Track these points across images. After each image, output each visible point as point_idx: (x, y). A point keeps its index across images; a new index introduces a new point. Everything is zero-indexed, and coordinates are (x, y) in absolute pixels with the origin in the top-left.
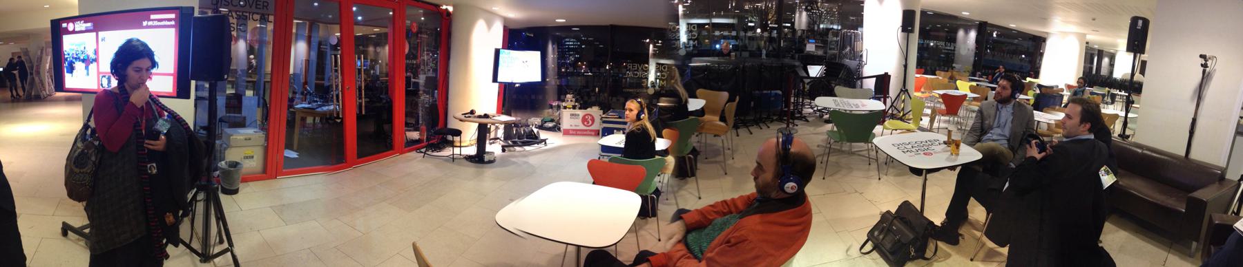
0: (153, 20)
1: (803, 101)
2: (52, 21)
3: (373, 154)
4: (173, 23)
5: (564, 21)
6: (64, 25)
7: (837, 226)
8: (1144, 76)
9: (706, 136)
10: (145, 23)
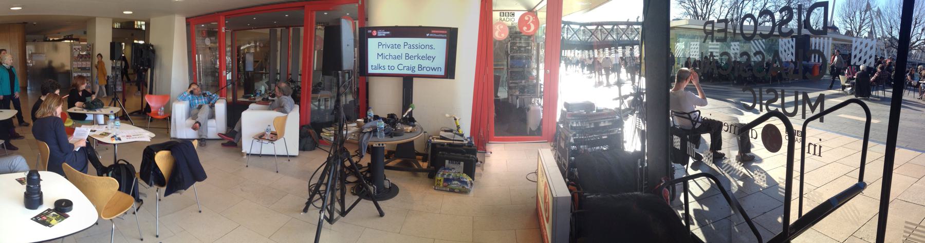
0: (433, 33)
2: (823, 122)
4: (445, 36)
5: (131, 13)
10: (428, 35)
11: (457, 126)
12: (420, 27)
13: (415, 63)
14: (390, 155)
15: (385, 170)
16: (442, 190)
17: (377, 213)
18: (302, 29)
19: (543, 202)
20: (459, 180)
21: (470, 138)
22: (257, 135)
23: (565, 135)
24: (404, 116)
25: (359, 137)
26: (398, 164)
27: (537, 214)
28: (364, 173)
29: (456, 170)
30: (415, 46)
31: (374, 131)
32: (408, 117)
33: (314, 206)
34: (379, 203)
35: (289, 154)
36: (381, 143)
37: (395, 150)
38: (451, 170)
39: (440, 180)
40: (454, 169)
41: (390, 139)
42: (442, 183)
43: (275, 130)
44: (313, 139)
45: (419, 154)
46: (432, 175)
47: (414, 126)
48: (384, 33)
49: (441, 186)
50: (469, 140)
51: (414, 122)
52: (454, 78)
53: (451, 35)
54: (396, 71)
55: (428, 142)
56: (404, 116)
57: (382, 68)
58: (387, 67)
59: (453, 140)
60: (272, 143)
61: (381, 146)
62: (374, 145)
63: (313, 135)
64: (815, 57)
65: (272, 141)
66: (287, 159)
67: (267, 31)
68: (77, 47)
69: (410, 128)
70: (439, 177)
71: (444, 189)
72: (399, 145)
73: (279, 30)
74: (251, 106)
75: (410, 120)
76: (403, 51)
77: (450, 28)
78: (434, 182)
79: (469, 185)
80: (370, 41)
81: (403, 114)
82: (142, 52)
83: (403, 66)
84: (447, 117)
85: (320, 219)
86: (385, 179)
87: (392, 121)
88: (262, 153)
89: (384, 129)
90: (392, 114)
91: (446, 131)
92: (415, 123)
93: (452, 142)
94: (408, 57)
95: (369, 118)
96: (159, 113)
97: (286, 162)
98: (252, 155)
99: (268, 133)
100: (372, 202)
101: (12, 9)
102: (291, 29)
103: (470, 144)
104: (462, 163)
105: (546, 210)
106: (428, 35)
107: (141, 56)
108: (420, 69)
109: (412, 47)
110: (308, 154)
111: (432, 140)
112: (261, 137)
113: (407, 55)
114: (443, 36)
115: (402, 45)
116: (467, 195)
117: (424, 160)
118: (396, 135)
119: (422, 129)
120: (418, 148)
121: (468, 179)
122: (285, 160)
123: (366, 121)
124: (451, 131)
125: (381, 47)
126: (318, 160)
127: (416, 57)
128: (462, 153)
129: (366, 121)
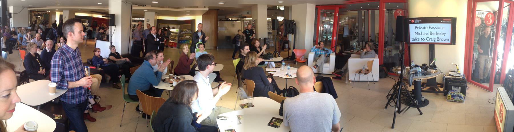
0: (444, 21)
1: (333, 38)
2: (12, 53)
3: (504, 127)
4: (450, 22)
8: (316, 82)
9: (393, 101)
10: (441, 22)
11: (457, 69)
12: (437, 17)
13: (435, 37)
14: (423, 85)
15: (422, 93)
16: (450, 101)
17: (419, 113)
18: (377, 12)
19: (499, 113)
20: (458, 96)
21: (464, 75)
22: (357, 71)
23: (512, 81)
24: (431, 65)
25: (408, 76)
26: (428, 89)
27: (494, 120)
29: (457, 91)
30: (435, 28)
31: (416, 73)
32: (433, 65)
33: (390, 105)
34: (420, 108)
35: (374, 80)
36: (420, 79)
37: (426, 82)
38: (454, 91)
39: (450, 96)
40: (456, 91)
41: (425, 77)
42: (450, 98)
43: (368, 69)
44: (385, 72)
45: (439, 84)
46: (445, 94)
47: (436, 70)
48: (418, 21)
49: (450, 99)
50: (463, 76)
51: (436, 68)
52: (455, 44)
53: (453, 21)
54: (425, 41)
55: (443, 78)
56: (431, 65)
57: (418, 39)
58: (420, 39)
59: (456, 76)
60: (366, 75)
61: (420, 80)
62: (416, 80)
63: (385, 70)
65: (366, 74)
66: (373, 83)
67: (356, 12)
68: (246, 22)
69: (434, 71)
70: (449, 95)
71: (452, 100)
72: (428, 80)
73: (363, 12)
74: (352, 55)
75: (434, 67)
76: (429, 30)
77: (453, 18)
78: (447, 98)
79: (463, 98)
81: (430, 64)
82: (289, 25)
83: (429, 38)
84: (452, 65)
85: (395, 111)
86: (422, 97)
87: (424, 68)
88: (360, 80)
89: (421, 72)
90: (424, 64)
91: (452, 72)
92: (437, 68)
93: (455, 77)
94: (432, 33)
95: (412, 66)
96: (301, 59)
97: (373, 84)
98: (355, 81)
99: (364, 70)
100: (416, 108)
102: (370, 11)
103: (463, 78)
104: (460, 88)
105: (500, 117)
106: (441, 22)
107: (289, 27)
108: (438, 40)
109: (433, 28)
110: (383, 80)
111: (445, 77)
112: (360, 72)
113: (431, 32)
114: (449, 22)
115: (428, 27)
116: (462, 103)
117: (441, 87)
118: (427, 75)
119: (440, 71)
120: (438, 81)
121: (463, 96)
122: (372, 84)
123: (411, 68)
124: (454, 72)
125: (417, 28)
126: (390, 84)
127: (436, 34)
128: (459, 82)
129: (411, 68)
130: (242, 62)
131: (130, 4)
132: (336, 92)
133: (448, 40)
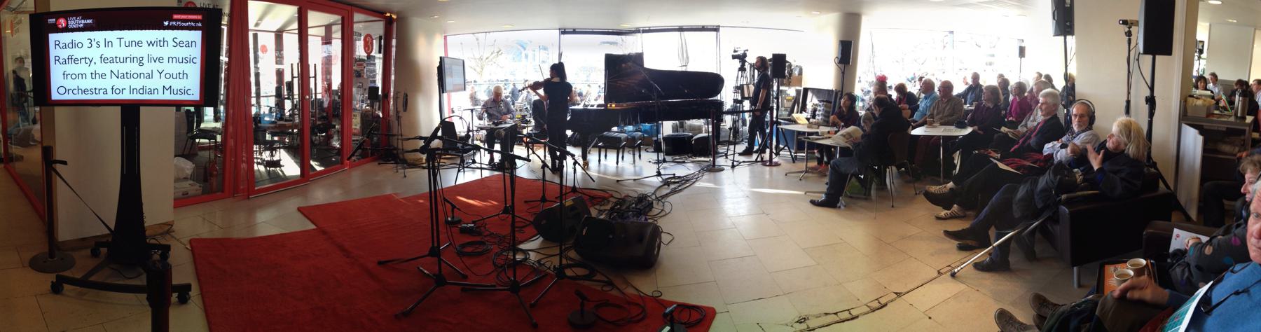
0: (176, 20)
6: (52, 21)
7: (883, 247)
10: (166, 23)
28: (759, 159)
64: (196, 21)
80: (53, 37)
101: (1212, 282)
130: (645, 123)
131: (642, 37)
132: (170, 326)
133: (84, 76)
